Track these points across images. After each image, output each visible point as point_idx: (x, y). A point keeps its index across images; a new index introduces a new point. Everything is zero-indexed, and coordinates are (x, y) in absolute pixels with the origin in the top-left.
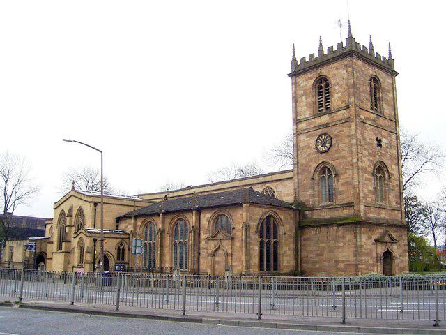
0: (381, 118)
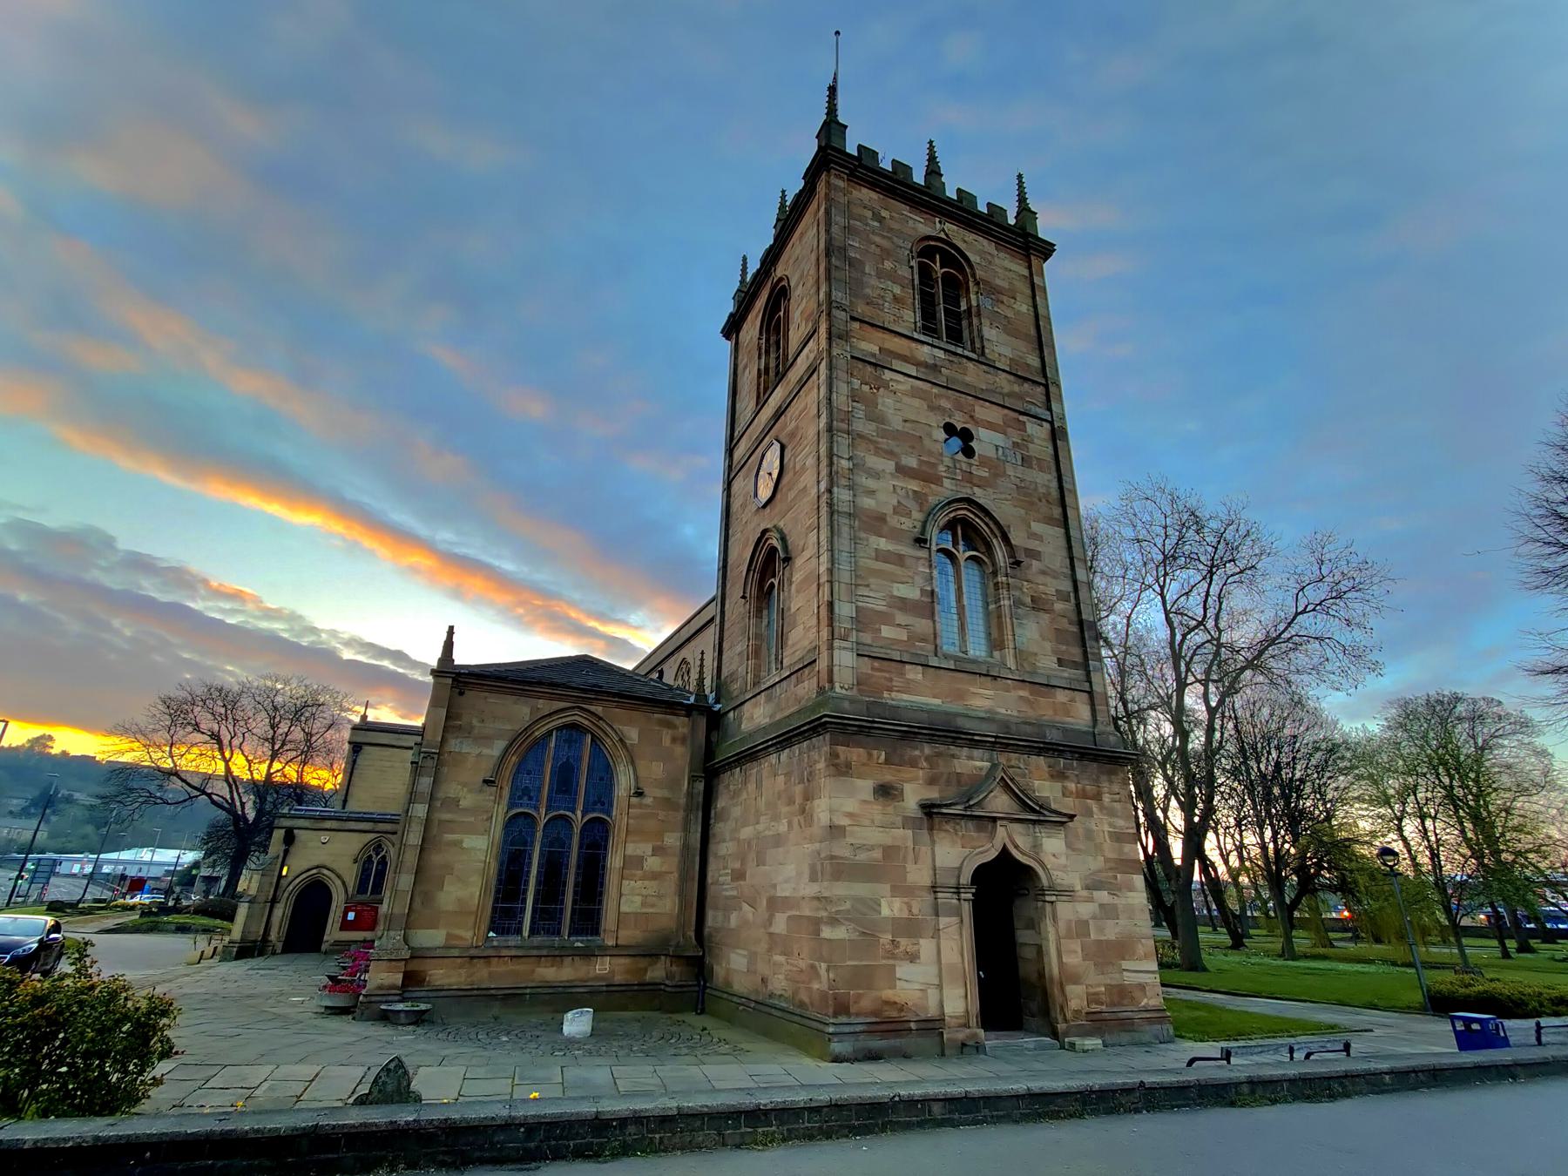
0: (970, 365)
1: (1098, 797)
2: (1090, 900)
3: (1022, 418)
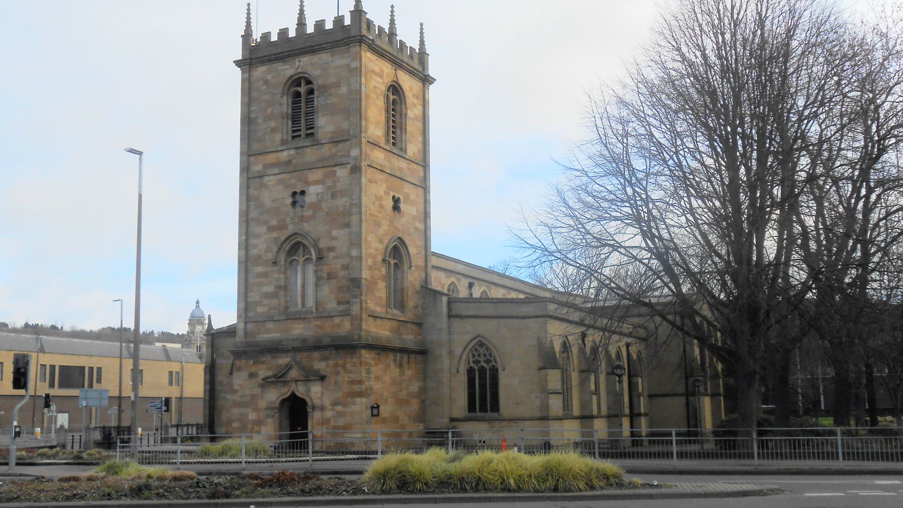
1: (344, 366)
2: (333, 410)
3: (334, 169)
